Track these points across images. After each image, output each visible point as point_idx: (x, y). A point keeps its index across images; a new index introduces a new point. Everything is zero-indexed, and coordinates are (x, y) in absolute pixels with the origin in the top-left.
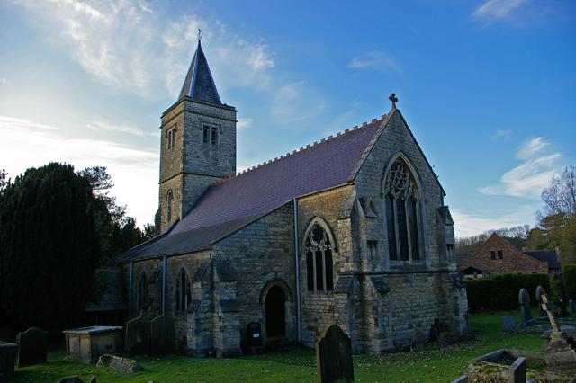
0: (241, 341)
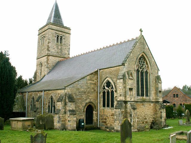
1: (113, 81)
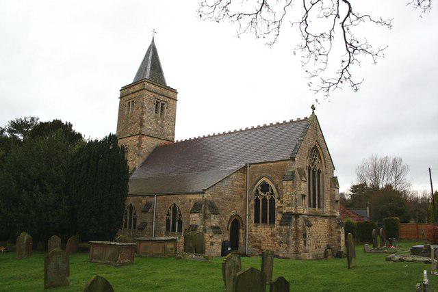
1: (273, 183)
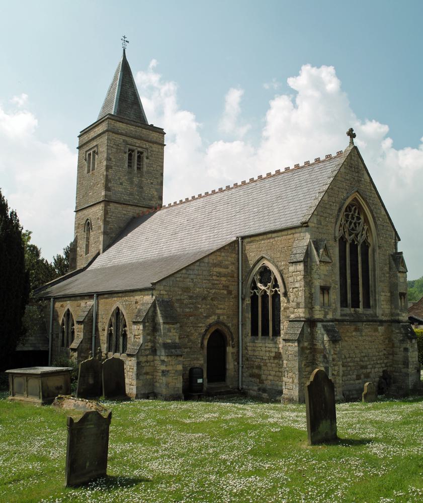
0: (183, 386)
1: (277, 267)
